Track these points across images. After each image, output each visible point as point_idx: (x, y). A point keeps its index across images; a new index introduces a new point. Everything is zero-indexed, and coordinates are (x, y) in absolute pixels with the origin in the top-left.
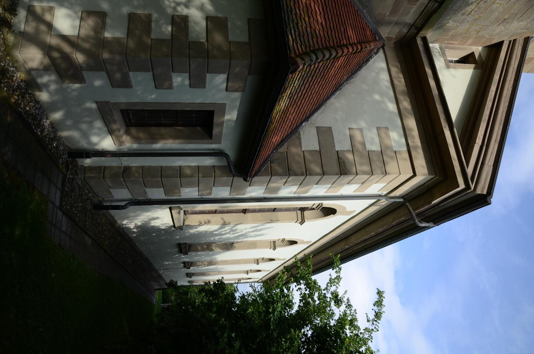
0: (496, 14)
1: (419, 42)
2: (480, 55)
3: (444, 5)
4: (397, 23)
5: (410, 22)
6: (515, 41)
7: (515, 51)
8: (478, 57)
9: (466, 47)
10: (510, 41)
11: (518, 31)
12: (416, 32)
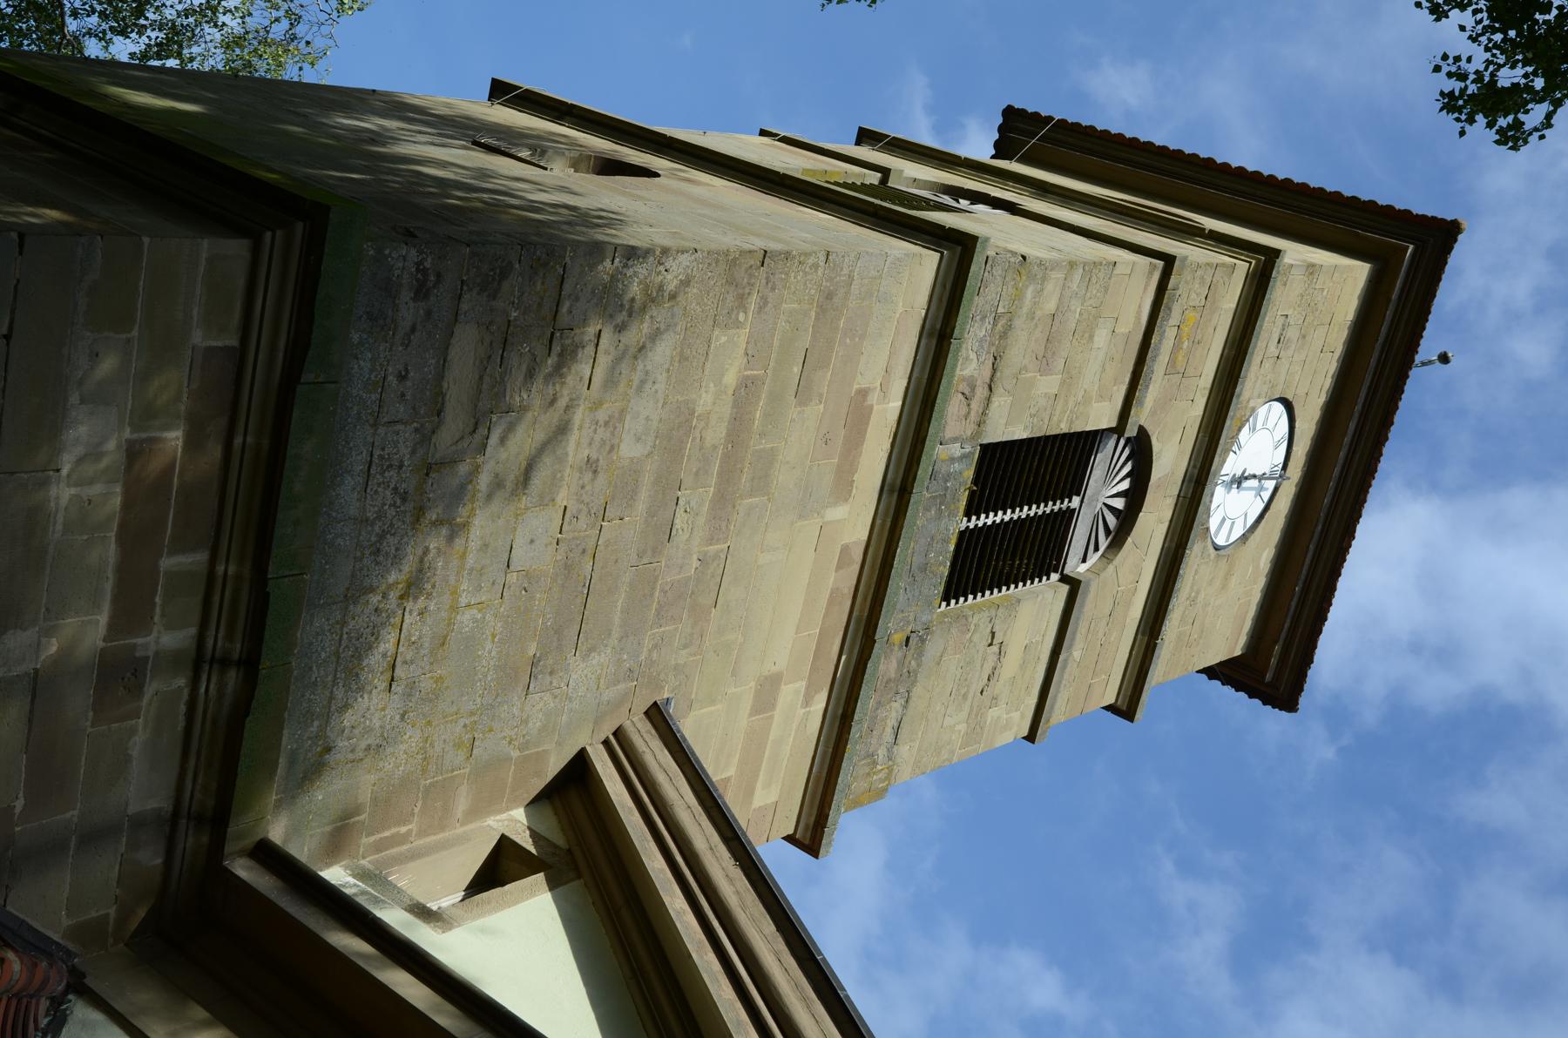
0: (489, 651)
1: (244, 870)
2: (534, 835)
3: (265, 664)
4: (93, 837)
5: (152, 804)
6: (619, 733)
7: (649, 759)
8: (535, 843)
9: (460, 830)
10: (606, 743)
11: (609, 694)
12: (205, 839)
